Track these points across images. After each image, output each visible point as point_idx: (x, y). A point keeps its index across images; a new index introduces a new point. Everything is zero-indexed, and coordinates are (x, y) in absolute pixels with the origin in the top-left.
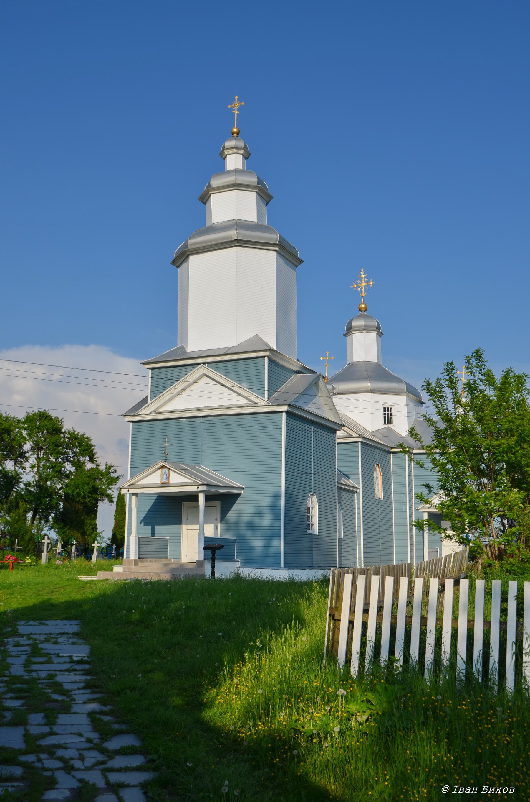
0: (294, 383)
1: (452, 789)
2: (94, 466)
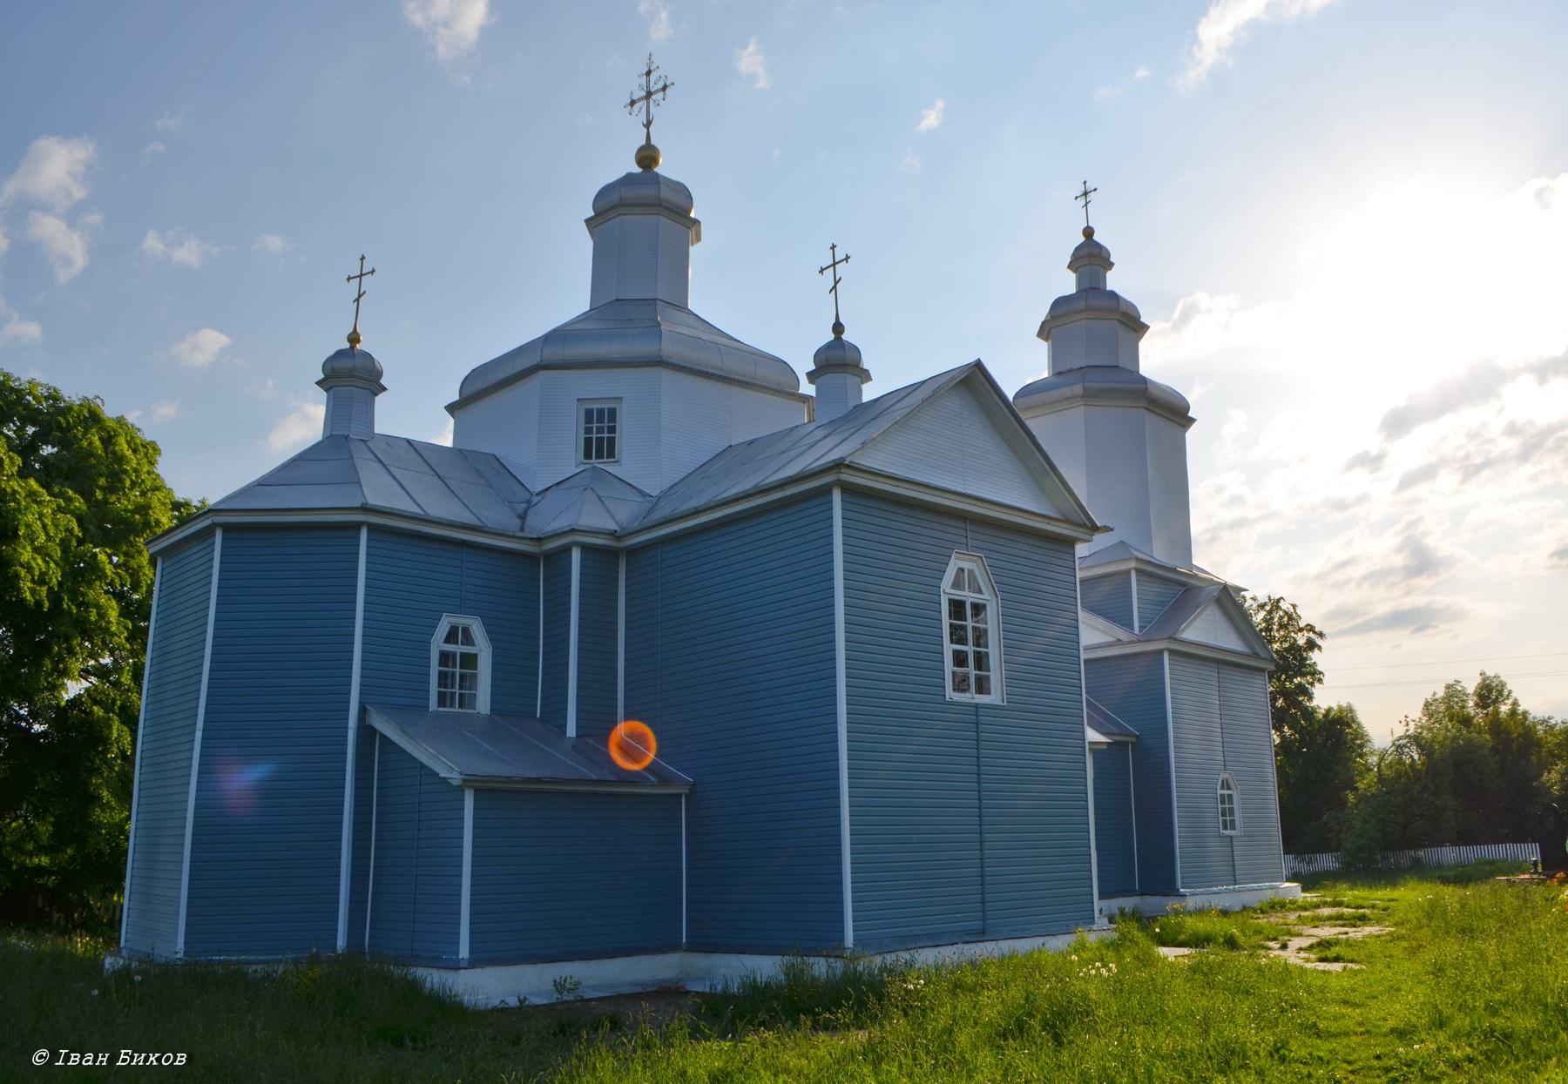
1: (55, 1055)
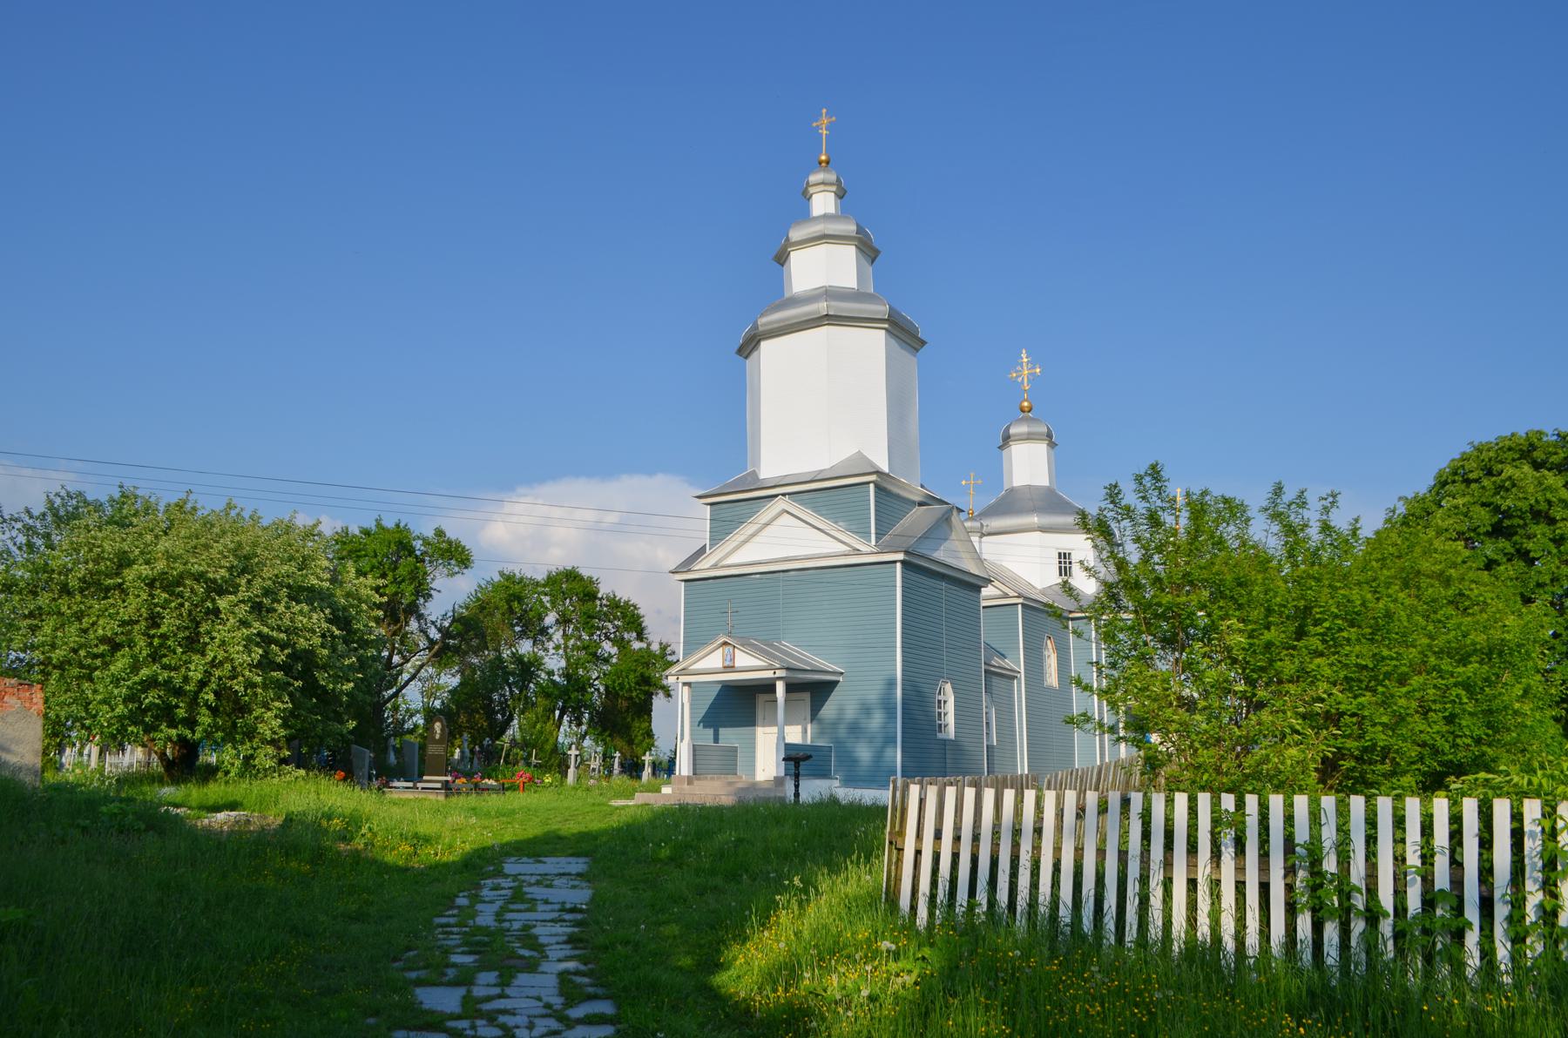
0: (916, 520)
2: (644, 645)
